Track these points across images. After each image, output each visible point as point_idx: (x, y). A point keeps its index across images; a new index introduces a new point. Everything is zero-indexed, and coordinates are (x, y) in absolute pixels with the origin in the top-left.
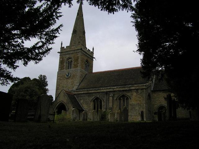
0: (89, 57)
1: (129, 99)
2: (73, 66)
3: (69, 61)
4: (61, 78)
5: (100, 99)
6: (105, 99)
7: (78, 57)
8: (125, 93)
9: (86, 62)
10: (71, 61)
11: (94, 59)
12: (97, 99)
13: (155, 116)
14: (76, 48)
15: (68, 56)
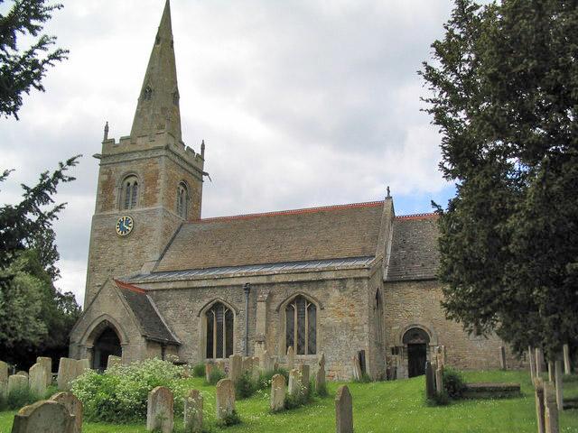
0: (190, 169)
1: (318, 309)
2: (140, 198)
3: (129, 184)
4: (105, 237)
5: (226, 308)
6: (242, 307)
8: (304, 290)
9: (182, 188)
10: (136, 184)
11: (205, 178)
12: (217, 306)
13: (394, 357)
14: (152, 146)
15: (125, 168)
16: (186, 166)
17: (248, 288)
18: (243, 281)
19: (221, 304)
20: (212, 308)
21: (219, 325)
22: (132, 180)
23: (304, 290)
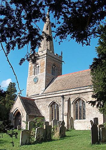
0: (57, 61)
3: (37, 67)
4: (31, 84)
5: (82, 100)
7: (44, 62)
8: (81, 96)
9: (54, 67)
10: (39, 66)
12: (54, 103)
16: (55, 59)
17: (63, 97)
18: (61, 94)
19: (55, 102)
20: (53, 104)
21: (55, 110)
22: (37, 66)
23: (81, 96)
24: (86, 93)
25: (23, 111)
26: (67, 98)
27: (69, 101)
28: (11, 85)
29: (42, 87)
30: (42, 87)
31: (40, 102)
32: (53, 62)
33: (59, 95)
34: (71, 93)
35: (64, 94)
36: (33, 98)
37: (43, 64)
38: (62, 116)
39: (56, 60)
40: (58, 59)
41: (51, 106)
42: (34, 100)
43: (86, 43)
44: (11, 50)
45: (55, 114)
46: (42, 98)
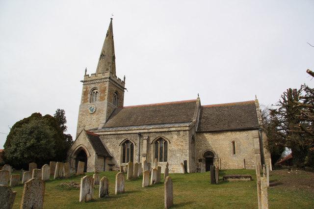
4: (84, 114)
7: (105, 88)
8: (163, 135)
10: (97, 92)
12: (127, 141)
17: (140, 135)
18: (138, 131)
21: (128, 149)
22: (95, 91)
23: (163, 135)
24: (169, 133)
25: (91, 149)
26: (145, 137)
27: (148, 140)
28: (59, 113)
29: (101, 118)
30: (101, 118)
31: (107, 139)
32: (115, 89)
33: (134, 132)
34: (150, 131)
35: (141, 131)
36: (97, 133)
37: (104, 91)
38: (137, 157)
39: (119, 87)
40: (121, 85)
41: (123, 145)
42: (99, 135)
43: (251, 142)
44: (83, 83)
45: (128, 154)
46: (111, 135)
